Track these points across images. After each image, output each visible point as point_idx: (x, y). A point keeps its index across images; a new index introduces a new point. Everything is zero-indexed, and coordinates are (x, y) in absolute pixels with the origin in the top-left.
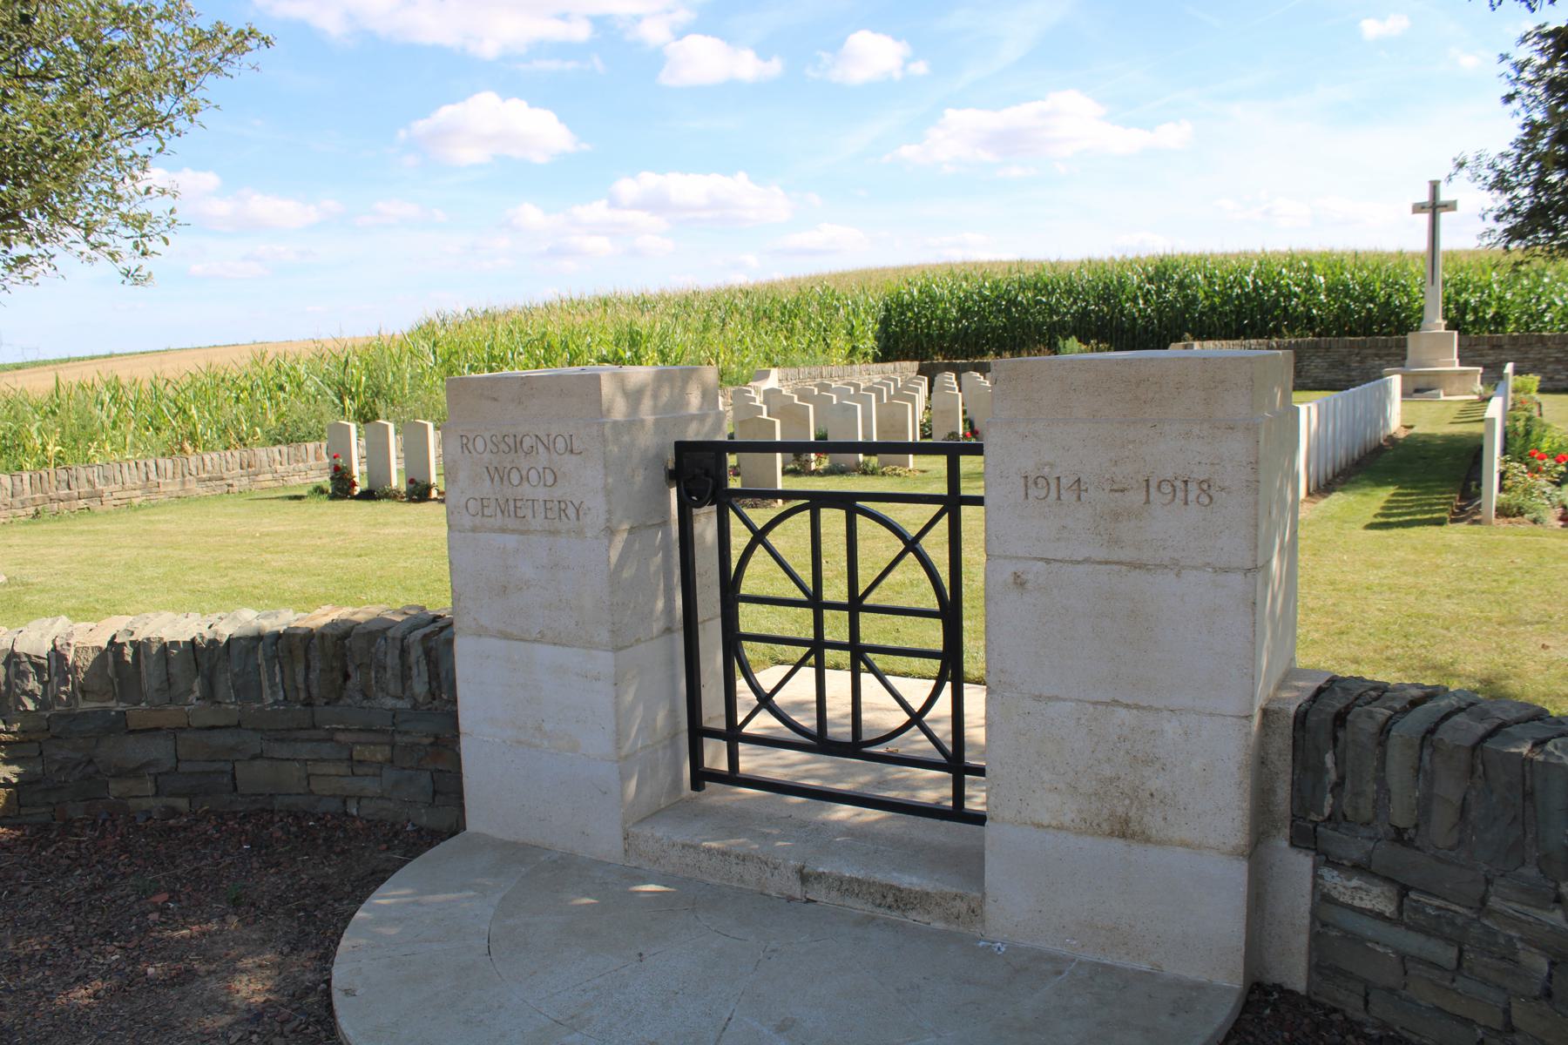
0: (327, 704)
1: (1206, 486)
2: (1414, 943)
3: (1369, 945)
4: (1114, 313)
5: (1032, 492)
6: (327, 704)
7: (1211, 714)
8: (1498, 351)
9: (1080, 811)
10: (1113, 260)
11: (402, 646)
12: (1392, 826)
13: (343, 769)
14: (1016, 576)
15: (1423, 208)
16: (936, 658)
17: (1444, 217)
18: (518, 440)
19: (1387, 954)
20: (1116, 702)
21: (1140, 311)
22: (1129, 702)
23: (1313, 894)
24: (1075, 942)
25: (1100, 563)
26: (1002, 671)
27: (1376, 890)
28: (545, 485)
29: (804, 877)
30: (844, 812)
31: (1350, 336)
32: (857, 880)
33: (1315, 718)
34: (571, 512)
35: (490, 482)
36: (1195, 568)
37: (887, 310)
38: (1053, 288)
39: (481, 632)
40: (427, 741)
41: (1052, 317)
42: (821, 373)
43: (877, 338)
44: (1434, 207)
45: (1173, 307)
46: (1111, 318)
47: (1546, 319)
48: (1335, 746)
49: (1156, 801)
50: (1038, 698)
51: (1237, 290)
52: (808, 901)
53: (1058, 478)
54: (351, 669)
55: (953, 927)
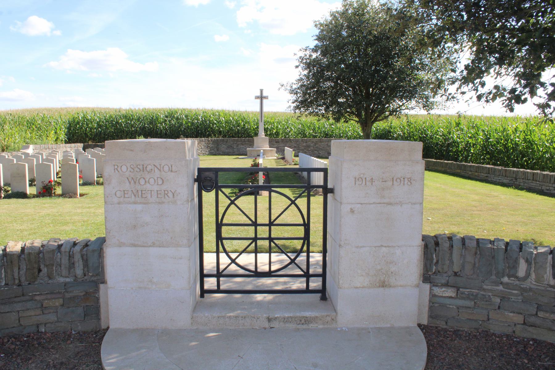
0: (29, 284)
1: (410, 180)
2: (461, 302)
3: (448, 306)
4: (154, 128)
5: (357, 183)
6: (29, 284)
7: (410, 246)
8: (278, 144)
9: (370, 281)
10: (139, 109)
11: (69, 255)
12: (453, 272)
13: (39, 312)
14: (351, 209)
15: (258, 97)
16: (302, 240)
17: (265, 101)
18: (145, 167)
19: (453, 308)
20: (382, 246)
21: (163, 127)
22: (386, 245)
23: (430, 295)
24: (367, 323)
25: (378, 204)
26: (346, 240)
27: (449, 290)
28: (158, 184)
29: (269, 320)
30: (259, 297)
31: (232, 137)
32: (291, 317)
33: (430, 245)
34: (170, 195)
35: (128, 184)
36: (406, 203)
37: (70, 124)
38: (132, 118)
39: (121, 245)
40: (82, 294)
41: (132, 129)
42: (49, 147)
43: (66, 134)
44: (262, 98)
45: (175, 126)
46: (153, 129)
47: (290, 134)
48: (436, 252)
49: (393, 274)
50: (357, 247)
51: (196, 121)
52: (271, 328)
53: (366, 178)
54: (42, 267)
55: (326, 326)
